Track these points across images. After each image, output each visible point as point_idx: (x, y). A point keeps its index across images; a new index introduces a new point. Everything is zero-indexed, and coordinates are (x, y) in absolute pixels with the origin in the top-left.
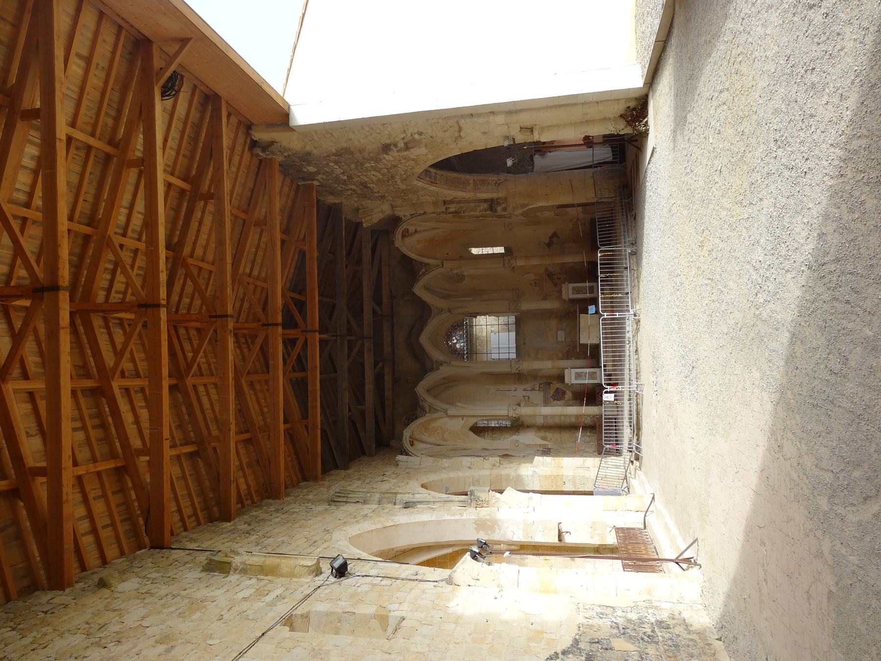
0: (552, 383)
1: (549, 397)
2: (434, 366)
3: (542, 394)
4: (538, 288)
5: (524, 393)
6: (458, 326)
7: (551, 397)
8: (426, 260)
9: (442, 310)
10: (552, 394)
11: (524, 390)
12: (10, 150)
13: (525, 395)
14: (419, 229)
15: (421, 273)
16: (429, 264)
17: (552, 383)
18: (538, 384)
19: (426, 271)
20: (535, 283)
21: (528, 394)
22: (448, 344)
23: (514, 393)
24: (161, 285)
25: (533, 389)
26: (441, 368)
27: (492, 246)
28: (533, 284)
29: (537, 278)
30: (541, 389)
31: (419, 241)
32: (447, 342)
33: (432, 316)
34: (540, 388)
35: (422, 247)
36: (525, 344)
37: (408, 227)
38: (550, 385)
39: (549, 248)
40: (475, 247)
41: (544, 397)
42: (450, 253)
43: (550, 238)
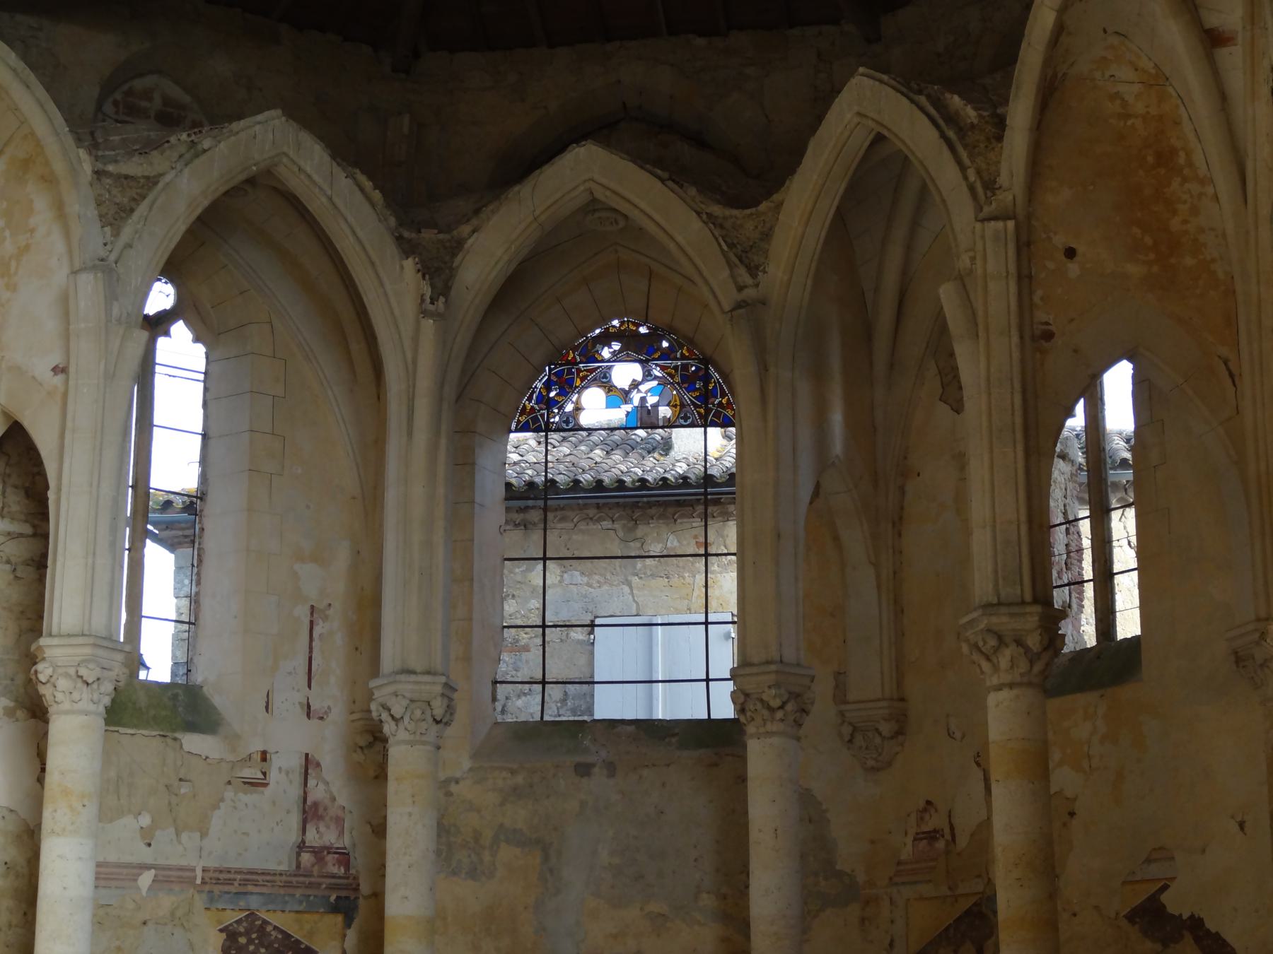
0: (348, 923)
1: (254, 903)
2: (428, 235)
3: (280, 862)
4: (907, 852)
5: (286, 762)
6: (705, 397)
7: (252, 916)
8: (1020, 113)
9: (753, 270)
10: (276, 919)
11: (309, 764)
12: (1139, 618)
13: (276, 762)
14: (1232, 58)
15: (956, 101)
16: (1000, 138)
17: (348, 923)
18: (346, 841)
19: (961, 131)
20: (932, 836)
21: (283, 784)
22: (606, 339)
23: (289, 697)
24: (1115, 544)
25: (310, 813)
26: (409, 264)
27: (1144, 568)
28: (935, 821)
29: (962, 841)
30: (306, 858)
31: (1157, 81)
32: (618, 336)
33: (717, 210)
34: (320, 853)
35: (1116, 96)
36: (584, 770)
37: (1240, 39)
38: (335, 909)
39: (1132, 917)
40: (1138, 516)
41: (251, 877)
42: (1073, 268)
43: (1196, 925)
